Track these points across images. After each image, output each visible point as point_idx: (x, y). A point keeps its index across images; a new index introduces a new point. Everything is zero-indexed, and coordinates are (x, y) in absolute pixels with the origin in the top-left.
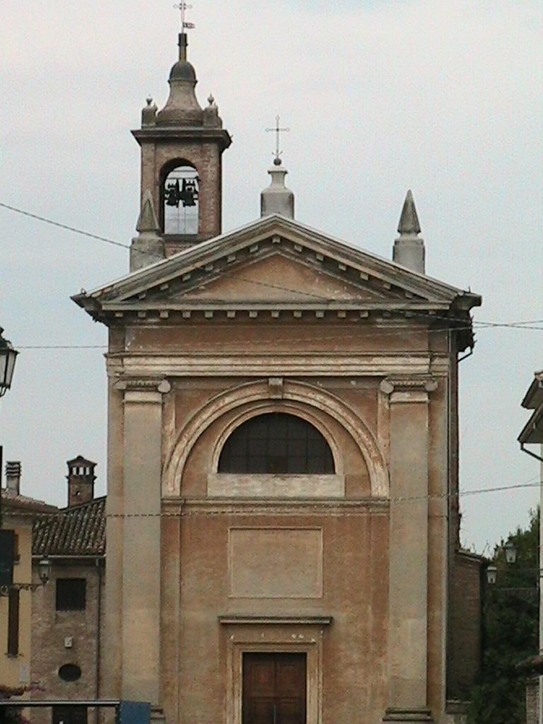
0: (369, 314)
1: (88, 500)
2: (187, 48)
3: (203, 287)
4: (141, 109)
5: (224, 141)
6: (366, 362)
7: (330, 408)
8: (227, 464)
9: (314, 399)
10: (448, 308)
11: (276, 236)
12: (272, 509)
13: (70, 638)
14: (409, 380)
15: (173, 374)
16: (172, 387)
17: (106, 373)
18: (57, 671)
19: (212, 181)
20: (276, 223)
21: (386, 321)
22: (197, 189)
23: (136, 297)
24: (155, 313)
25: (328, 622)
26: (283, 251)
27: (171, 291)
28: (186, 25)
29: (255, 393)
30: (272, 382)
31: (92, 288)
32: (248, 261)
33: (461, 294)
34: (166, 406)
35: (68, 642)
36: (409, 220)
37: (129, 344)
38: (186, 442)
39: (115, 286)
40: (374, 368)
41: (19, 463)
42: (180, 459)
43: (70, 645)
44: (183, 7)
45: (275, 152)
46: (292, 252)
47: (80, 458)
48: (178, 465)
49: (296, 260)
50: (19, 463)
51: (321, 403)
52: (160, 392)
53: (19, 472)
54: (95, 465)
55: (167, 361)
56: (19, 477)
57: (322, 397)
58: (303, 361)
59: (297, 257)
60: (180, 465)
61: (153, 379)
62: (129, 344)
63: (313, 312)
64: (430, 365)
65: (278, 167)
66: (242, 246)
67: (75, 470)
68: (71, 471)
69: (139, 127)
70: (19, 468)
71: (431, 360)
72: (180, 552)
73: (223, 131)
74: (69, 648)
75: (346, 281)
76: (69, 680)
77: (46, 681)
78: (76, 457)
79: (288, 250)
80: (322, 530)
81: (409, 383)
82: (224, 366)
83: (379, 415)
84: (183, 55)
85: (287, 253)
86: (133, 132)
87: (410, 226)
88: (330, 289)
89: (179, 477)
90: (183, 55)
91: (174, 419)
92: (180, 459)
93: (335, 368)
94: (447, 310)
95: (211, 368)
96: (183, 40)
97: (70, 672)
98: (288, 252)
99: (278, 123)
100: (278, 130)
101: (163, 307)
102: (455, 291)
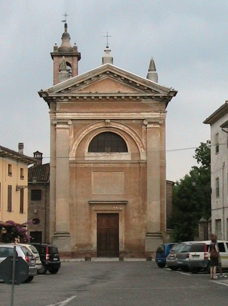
5: (79, 58)
11: (108, 71)
23: (60, 92)
26: (110, 77)
27: (72, 90)
36: (152, 66)
37: (58, 108)
40: (141, 116)
43: (36, 212)
44: (66, 15)
55: (70, 114)
61: (66, 120)
67: (36, 156)
69: (52, 52)
74: (35, 213)
82: (91, 116)
84: (66, 30)
90: (66, 30)
93: (128, 116)
95: (86, 116)
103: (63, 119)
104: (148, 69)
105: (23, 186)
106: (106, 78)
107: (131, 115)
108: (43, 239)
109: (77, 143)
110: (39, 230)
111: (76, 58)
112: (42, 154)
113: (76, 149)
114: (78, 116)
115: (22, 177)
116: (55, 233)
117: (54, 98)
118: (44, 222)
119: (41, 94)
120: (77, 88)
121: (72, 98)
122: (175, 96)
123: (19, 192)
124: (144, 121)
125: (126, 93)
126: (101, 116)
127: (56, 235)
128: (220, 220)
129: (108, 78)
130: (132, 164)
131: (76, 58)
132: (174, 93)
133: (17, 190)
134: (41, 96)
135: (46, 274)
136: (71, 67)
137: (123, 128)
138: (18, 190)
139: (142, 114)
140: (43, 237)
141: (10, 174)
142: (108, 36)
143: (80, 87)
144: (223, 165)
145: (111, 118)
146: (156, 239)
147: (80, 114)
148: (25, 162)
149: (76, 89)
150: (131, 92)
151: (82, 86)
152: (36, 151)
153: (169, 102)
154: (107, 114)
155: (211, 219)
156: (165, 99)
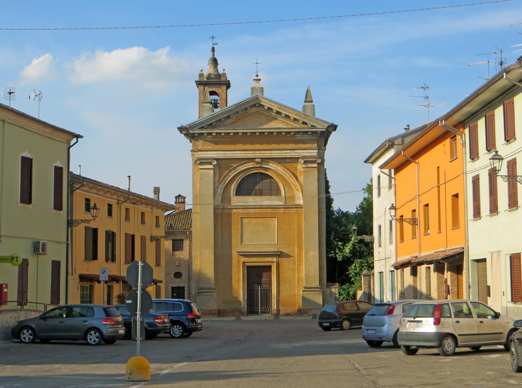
1: (183, 210)
3: (229, 124)
4: (146, 236)
5: (228, 85)
7: (279, 170)
8: (238, 193)
10: (325, 130)
11: (258, 103)
12: (257, 210)
14: (310, 159)
15: (217, 157)
16: (217, 163)
20: (257, 98)
21: (300, 136)
22: (219, 102)
23: (203, 127)
25: (280, 253)
27: (216, 125)
28: (214, 44)
29: (250, 165)
30: (257, 160)
31: (185, 123)
32: (246, 113)
33: (330, 124)
36: (308, 99)
37: (200, 146)
38: (223, 184)
39: (195, 123)
40: (296, 154)
41: (159, 188)
46: (263, 110)
47: (180, 196)
48: (220, 193)
51: (275, 168)
52: (213, 165)
53: (159, 192)
54: (185, 197)
55: (215, 152)
56: (159, 194)
57: (276, 166)
58: (268, 152)
60: (221, 193)
61: (210, 159)
62: (200, 146)
63: (272, 133)
64: (318, 153)
65: (257, 77)
67: (178, 200)
68: (176, 200)
69: (198, 80)
70: (159, 190)
72: (222, 227)
76: (177, 278)
78: (178, 195)
79: (262, 109)
81: (310, 160)
82: (238, 154)
83: (298, 172)
86: (196, 81)
89: (220, 198)
91: (218, 175)
93: (281, 154)
94: (324, 131)
95: (232, 155)
96: (213, 50)
97: (178, 275)
98: (262, 110)
99: (257, 61)
100: (257, 63)
104: (304, 100)
105: (158, 236)
107: (283, 153)
108: (186, 296)
109: (223, 185)
111: (224, 88)
113: (221, 193)
114: (224, 155)
115: (157, 225)
117: (196, 135)
119: (181, 129)
120: (222, 123)
121: (216, 134)
124: (299, 160)
125: (279, 128)
126: (250, 155)
127: (200, 291)
128: (383, 272)
133: (152, 241)
134: (181, 132)
135: (331, 331)
136: (219, 96)
138: (153, 241)
139: (297, 152)
142: (256, 64)
144: (385, 211)
145: (262, 157)
146: (316, 294)
148: (162, 209)
150: (284, 127)
151: (228, 121)
152: (178, 195)
154: (257, 152)
155: (374, 271)
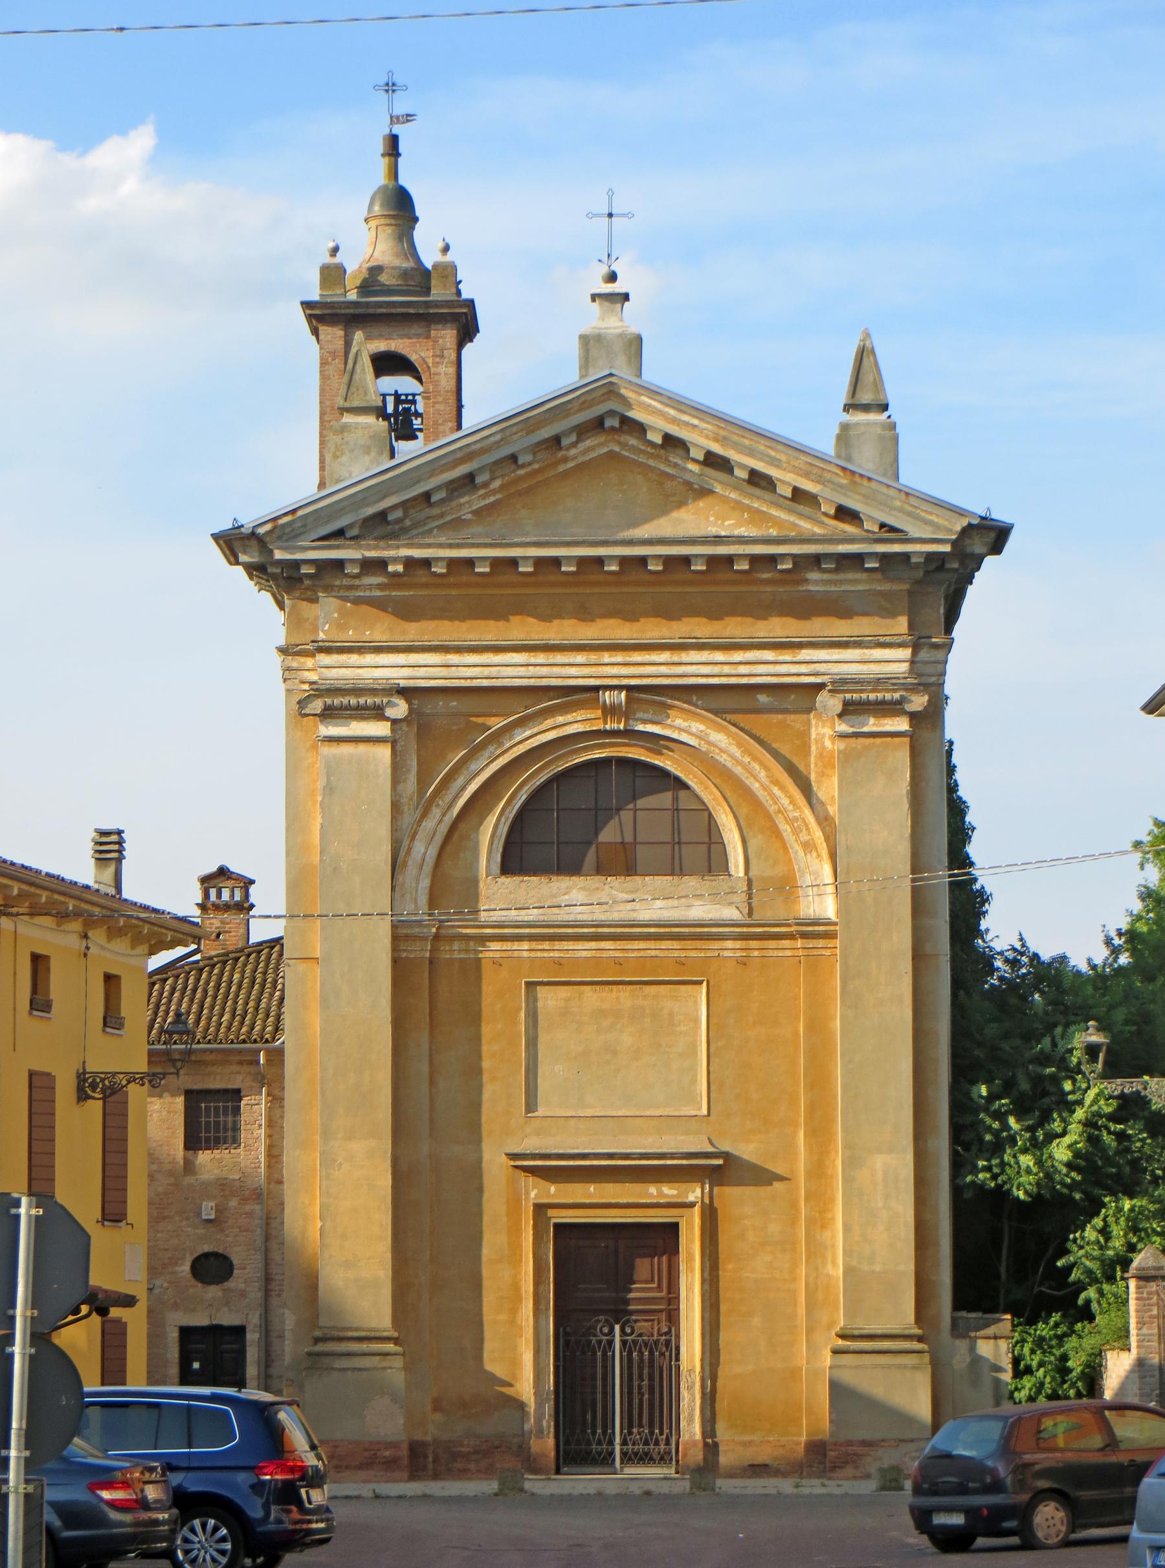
0: (795, 563)
2: (400, 160)
3: (469, 516)
6: (788, 658)
9: (686, 731)
10: (947, 548)
11: (612, 413)
13: (212, 1204)
14: (872, 691)
17: (282, 687)
18: (186, 1267)
19: (448, 391)
20: (609, 389)
21: (826, 576)
23: (340, 533)
24: (380, 565)
25: (720, 1162)
26: (624, 445)
27: (408, 523)
28: (394, 119)
30: (608, 697)
34: (400, 743)
35: (208, 1210)
38: (438, 817)
39: (300, 513)
40: (803, 669)
41: (120, 833)
42: (427, 849)
43: (212, 1217)
44: (390, 87)
45: (605, 259)
49: (651, 463)
50: (120, 833)
52: (387, 719)
53: (120, 852)
54: (252, 882)
56: (119, 860)
58: (665, 656)
59: (651, 456)
61: (373, 691)
64: (912, 662)
66: (546, 433)
68: (206, 895)
69: (315, 295)
70: (120, 843)
71: (914, 654)
73: (466, 300)
74: (209, 1221)
75: (746, 501)
77: (165, 1285)
80: (705, 984)
81: (872, 696)
83: (813, 759)
84: (394, 172)
85: (634, 449)
87: (865, 397)
88: (717, 519)
89: (425, 883)
90: (394, 172)
92: (427, 849)
93: (727, 669)
96: (393, 146)
98: (633, 446)
100: (610, 215)
101: (392, 553)
102: (960, 512)
103: (358, 691)
105: (114, 1074)
106: (604, 450)
108: (251, 1371)
109: (440, 821)
110: (228, 1319)
111: (448, 336)
112: (247, 883)
115: (112, 1019)
116: (318, 1333)
117: (305, 570)
118: (260, 1274)
120: (436, 511)
122: (997, 547)
123: (95, 1107)
124: (819, 698)
125: (718, 540)
127: (320, 1347)
129: (611, 455)
130: (754, 944)
131: (448, 336)
132: (993, 535)
133: (82, 1096)
136: (419, 379)
137: (697, 737)
138: (89, 1097)
140: (252, 1354)
141: (40, 1003)
142: (613, 212)
143: (454, 504)
145: (633, 682)
147: (454, 658)
149: (433, 518)
152: (213, 868)
153: (970, 588)
154: (606, 657)
156: (941, 568)
